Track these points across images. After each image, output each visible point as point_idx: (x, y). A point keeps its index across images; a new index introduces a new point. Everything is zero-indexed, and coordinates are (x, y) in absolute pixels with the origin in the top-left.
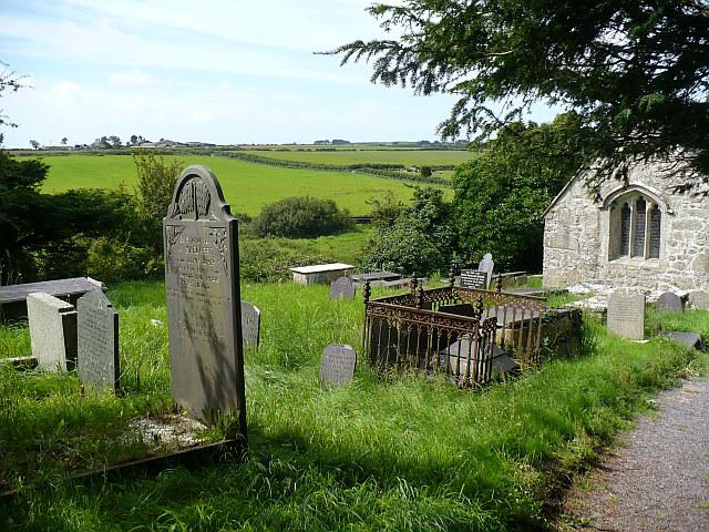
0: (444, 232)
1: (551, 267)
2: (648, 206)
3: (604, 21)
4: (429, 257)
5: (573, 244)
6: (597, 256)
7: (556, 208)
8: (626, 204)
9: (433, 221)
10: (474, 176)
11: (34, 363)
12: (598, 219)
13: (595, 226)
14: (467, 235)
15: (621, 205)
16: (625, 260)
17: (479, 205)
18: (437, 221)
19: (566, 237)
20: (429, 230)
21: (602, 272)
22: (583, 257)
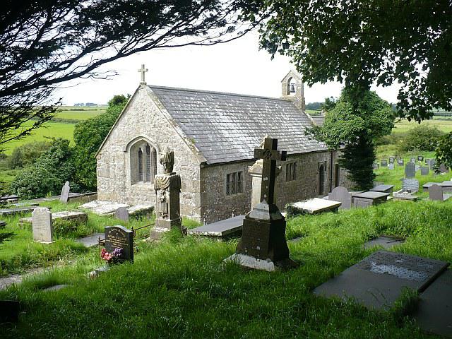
0: (67, 166)
1: (102, 189)
2: (151, 149)
3: (371, 21)
4: (48, 183)
5: (112, 175)
6: (125, 182)
7: (102, 152)
8: (140, 149)
9: (60, 160)
10: (85, 130)
11: (336, 186)
12: (124, 158)
13: (122, 163)
14: (81, 168)
15: (137, 149)
16: (141, 185)
17: (87, 150)
18: (64, 159)
19: (108, 171)
20: (57, 165)
21: (128, 192)
22: (118, 183)
